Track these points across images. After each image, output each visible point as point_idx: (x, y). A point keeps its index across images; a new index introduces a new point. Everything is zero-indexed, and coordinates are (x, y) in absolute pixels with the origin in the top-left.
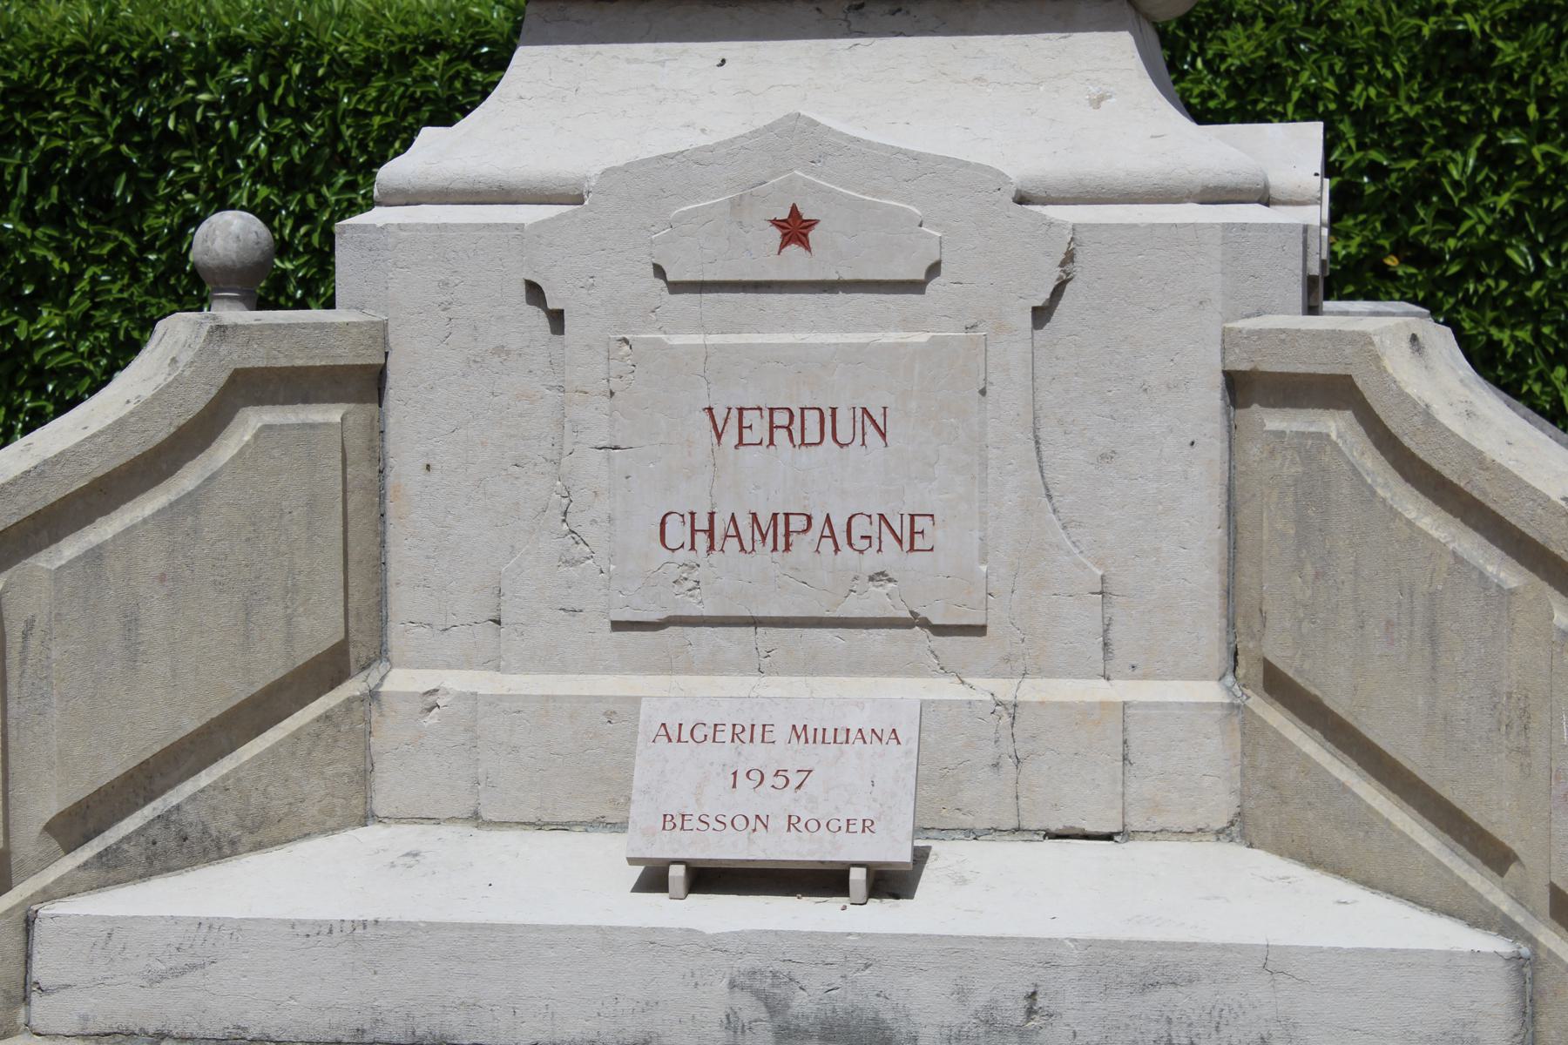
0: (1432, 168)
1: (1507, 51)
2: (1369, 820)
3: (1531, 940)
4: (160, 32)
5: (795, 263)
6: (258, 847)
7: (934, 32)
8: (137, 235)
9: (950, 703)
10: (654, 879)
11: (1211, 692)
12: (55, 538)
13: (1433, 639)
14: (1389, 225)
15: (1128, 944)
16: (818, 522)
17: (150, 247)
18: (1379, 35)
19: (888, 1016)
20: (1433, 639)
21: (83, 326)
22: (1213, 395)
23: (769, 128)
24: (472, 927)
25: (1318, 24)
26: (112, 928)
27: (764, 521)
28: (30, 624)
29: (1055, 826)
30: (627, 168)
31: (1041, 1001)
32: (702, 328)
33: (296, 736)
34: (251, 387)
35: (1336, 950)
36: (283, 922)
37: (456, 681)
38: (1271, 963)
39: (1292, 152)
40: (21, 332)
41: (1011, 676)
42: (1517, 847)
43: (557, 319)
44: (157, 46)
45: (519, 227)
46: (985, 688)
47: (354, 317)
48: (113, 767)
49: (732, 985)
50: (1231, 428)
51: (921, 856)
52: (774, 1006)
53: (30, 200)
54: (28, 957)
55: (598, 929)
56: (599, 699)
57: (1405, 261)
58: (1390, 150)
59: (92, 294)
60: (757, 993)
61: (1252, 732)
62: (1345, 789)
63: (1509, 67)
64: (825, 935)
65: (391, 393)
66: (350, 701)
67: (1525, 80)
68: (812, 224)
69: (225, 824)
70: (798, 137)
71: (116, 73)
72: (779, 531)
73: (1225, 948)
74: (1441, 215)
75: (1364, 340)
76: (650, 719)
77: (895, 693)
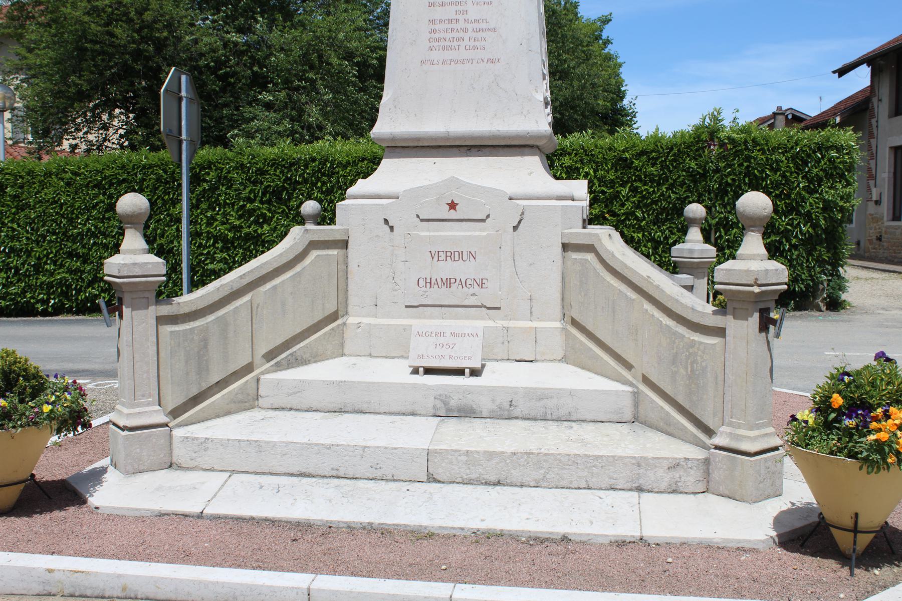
0: (617, 192)
1: (636, 163)
2: (597, 357)
3: (637, 388)
4: (295, 156)
5: (453, 214)
6: (315, 362)
8: (288, 207)
10: (415, 371)
11: (558, 325)
12: (265, 283)
13: (614, 312)
16: (458, 281)
17: (290, 210)
20: (614, 312)
26: (279, 382)
27: (444, 280)
28: (258, 305)
30: (410, 190)
32: (429, 231)
33: (325, 334)
37: (366, 320)
38: (572, 393)
39: (579, 187)
43: (392, 228)
46: (500, 323)
48: (279, 341)
50: (563, 257)
51: (483, 366)
53: (262, 198)
58: (607, 187)
60: (441, 400)
67: (641, 170)
69: (307, 356)
71: (284, 166)
72: (448, 283)
77: (479, 324)
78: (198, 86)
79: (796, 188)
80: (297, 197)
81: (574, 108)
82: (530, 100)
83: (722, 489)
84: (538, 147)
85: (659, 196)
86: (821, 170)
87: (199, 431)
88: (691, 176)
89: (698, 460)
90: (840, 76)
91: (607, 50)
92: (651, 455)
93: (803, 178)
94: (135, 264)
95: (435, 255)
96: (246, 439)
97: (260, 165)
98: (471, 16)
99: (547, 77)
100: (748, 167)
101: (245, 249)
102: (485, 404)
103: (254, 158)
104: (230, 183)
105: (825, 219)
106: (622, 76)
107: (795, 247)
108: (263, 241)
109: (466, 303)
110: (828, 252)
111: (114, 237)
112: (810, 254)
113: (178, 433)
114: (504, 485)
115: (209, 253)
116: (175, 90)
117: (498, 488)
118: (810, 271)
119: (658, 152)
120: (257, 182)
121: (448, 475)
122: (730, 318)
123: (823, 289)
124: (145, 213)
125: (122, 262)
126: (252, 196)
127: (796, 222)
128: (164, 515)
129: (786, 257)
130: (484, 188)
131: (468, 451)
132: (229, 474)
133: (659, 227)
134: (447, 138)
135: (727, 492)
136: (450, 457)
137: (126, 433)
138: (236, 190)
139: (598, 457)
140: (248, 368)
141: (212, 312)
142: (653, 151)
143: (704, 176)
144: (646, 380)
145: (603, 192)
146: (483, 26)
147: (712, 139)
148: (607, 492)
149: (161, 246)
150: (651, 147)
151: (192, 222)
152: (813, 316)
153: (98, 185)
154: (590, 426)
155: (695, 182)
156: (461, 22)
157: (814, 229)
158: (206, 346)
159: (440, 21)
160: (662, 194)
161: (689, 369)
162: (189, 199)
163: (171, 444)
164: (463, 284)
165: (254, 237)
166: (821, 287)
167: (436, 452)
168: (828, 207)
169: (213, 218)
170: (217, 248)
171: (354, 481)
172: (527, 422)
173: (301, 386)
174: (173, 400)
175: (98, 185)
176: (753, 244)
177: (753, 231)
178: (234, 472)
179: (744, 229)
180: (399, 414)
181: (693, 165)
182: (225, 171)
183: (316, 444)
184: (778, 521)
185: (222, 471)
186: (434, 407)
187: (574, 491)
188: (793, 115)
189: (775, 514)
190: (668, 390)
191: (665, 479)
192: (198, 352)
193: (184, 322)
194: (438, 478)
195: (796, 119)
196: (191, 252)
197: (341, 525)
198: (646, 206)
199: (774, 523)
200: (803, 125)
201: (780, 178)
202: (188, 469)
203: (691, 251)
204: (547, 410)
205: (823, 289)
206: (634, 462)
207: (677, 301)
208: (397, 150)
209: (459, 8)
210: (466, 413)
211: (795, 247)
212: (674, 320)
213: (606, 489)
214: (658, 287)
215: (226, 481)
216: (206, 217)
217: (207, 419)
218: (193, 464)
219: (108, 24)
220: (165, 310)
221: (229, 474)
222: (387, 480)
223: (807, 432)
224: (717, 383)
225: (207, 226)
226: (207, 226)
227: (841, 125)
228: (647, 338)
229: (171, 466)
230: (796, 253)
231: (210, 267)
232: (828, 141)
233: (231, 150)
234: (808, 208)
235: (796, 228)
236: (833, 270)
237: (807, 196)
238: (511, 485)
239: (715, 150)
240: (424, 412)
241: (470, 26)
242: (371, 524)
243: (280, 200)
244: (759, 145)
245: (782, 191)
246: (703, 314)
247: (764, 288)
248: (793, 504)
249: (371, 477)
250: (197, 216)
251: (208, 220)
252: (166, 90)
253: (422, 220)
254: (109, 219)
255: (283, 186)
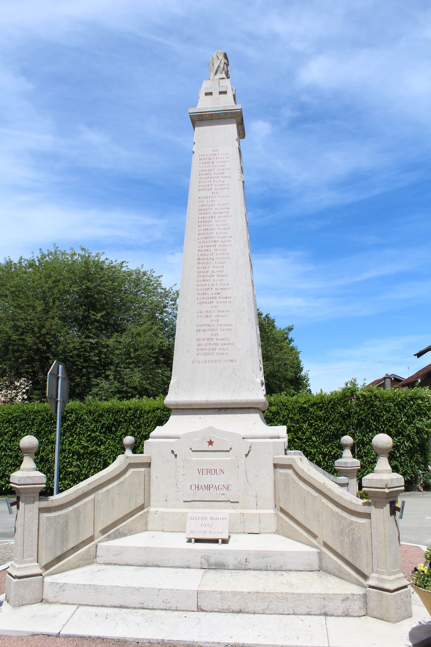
0: (301, 426)
1: (311, 410)
2: (296, 531)
3: (320, 549)
4: (120, 407)
5: (211, 448)
6: (131, 535)
7: (230, 414)
8: (115, 436)
9: (234, 513)
10: (190, 541)
11: (272, 511)
12: (102, 488)
13: (305, 504)
14: (295, 434)
15: (261, 551)
16: (214, 486)
17: (117, 437)
18: (293, 407)
19: (225, 562)
20: (305, 504)
21: (107, 449)
22: (272, 467)
23: (207, 428)
24: (162, 548)
25: (284, 406)
26: (109, 547)
27: (206, 486)
28: (98, 501)
29: (250, 532)
30: (186, 434)
31: (248, 560)
32: (197, 457)
33: (136, 518)
34: (131, 465)
35: (292, 552)
36: (134, 547)
37: (160, 510)
38: (282, 554)
39: (281, 430)
40: (98, 449)
41: (242, 509)
42: (318, 535)
43: (176, 456)
44: (119, 408)
45: (171, 442)
46: (239, 511)
47: (146, 455)
48: (110, 522)
49: (201, 557)
50: (274, 472)
51: (229, 537)
52: (207, 561)
53: (100, 431)
54: (96, 551)
55: (181, 549)
56: (181, 513)
57: (298, 440)
58: (295, 423)
59: (109, 444)
60: (205, 559)
61: (278, 517)
62: (292, 526)
63: (311, 412)
64: (215, 550)
65: (151, 466)
66: (145, 512)
67: (314, 414)
68: (213, 442)
69: (126, 531)
70: (211, 429)
71: (114, 412)
72: (208, 487)
73: (275, 551)
74: (302, 433)
75: (294, 459)
76: (189, 515)
77: (226, 512)
78: (67, 370)
79: (400, 421)
80: (120, 430)
81: (274, 376)
82: (253, 383)
83: (375, 613)
84: (258, 408)
85: (325, 428)
86: (414, 411)
87: (60, 578)
88: (342, 416)
89: (360, 595)
90: (418, 357)
91: (291, 345)
92: (331, 592)
93: (404, 415)
94: (28, 477)
95: (201, 471)
96: (88, 584)
97: (101, 412)
98: (220, 336)
99: (262, 370)
100: (373, 410)
101: (90, 460)
102: (231, 561)
103: (97, 408)
104: (83, 421)
105: (418, 438)
106: (300, 358)
107: (402, 454)
108: (100, 455)
109: (219, 499)
110: (421, 457)
111: (16, 451)
112: (411, 458)
113: (48, 579)
114: (244, 613)
115: (69, 461)
116: (56, 373)
117: (240, 615)
118: (412, 468)
119: (323, 403)
120: (98, 421)
121: (210, 606)
122: (373, 507)
123: (421, 479)
124: (36, 447)
125: (21, 476)
126: (95, 429)
127: (401, 441)
128: (36, 635)
129: (398, 461)
130: (228, 432)
131: (221, 592)
132: (77, 606)
133: (325, 446)
134: (207, 404)
135: (378, 616)
136: (211, 595)
137: (16, 580)
138: (86, 425)
139: (300, 594)
140: (91, 539)
141: (71, 505)
142: (320, 403)
143: (349, 416)
144: (326, 545)
145: (293, 427)
146: (227, 342)
147: (352, 395)
148: (306, 616)
149: (42, 457)
150: (318, 401)
151: (61, 443)
152: (416, 495)
153: (9, 421)
154: (294, 574)
155: (344, 419)
156: (215, 339)
157: (412, 444)
158: (67, 526)
159: (203, 339)
160: (327, 427)
161: (351, 538)
162: (60, 431)
163: (43, 587)
164: (217, 488)
165: (95, 453)
166: (419, 477)
167: (203, 592)
168: (419, 431)
169: (72, 442)
170: (74, 459)
171: (153, 611)
172: (256, 572)
173: (122, 550)
174: (45, 559)
175: (9, 421)
176: (383, 464)
177: (382, 456)
178: (80, 605)
179: (377, 455)
180: (180, 567)
181: (342, 410)
182: (80, 415)
183: (131, 588)
184: (412, 635)
185: (73, 604)
186: (201, 563)
187: (286, 616)
188: (395, 378)
189: (409, 630)
190: (339, 551)
191: (340, 607)
192: (62, 529)
193: (55, 511)
194: (204, 609)
195: (396, 381)
196: (60, 461)
197: (145, 641)
198: (318, 433)
199: (410, 637)
200: (401, 383)
201: (391, 416)
202: (52, 603)
203: (346, 463)
204: (268, 565)
205: (421, 479)
206: (321, 597)
207: (341, 497)
208: (179, 411)
209: (213, 332)
210: (220, 566)
211: (402, 454)
212: (340, 508)
213: (305, 615)
214: (330, 489)
215: (75, 611)
216: (69, 440)
217: (65, 571)
218: (55, 600)
219: (22, 334)
220: (44, 504)
221: (77, 606)
222: (173, 610)
223: (424, 578)
224: (367, 547)
225: (69, 446)
226: (69, 446)
227: (422, 385)
228: (325, 520)
229: (42, 601)
230: (403, 458)
231: (70, 470)
232: (416, 395)
233: (85, 404)
234: (408, 432)
235: (402, 444)
236: (425, 467)
237: (407, 425)
238: (248, 613)
239: (354, 402)
240: (195, 566)
241: (219, 342)
242: (163, 640)
243: (111, 431)
244: (378, 398)
245: (393, 423)
246: (357, 505)
247: (391, 490)
248: (420, 623)
249: (163, 608)
250: (63, 440)
251: (69, 443)
252: (51, 373)
253: (193, 451)
254: (14, 441)
255: (113, 424)
